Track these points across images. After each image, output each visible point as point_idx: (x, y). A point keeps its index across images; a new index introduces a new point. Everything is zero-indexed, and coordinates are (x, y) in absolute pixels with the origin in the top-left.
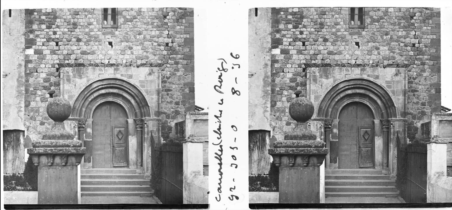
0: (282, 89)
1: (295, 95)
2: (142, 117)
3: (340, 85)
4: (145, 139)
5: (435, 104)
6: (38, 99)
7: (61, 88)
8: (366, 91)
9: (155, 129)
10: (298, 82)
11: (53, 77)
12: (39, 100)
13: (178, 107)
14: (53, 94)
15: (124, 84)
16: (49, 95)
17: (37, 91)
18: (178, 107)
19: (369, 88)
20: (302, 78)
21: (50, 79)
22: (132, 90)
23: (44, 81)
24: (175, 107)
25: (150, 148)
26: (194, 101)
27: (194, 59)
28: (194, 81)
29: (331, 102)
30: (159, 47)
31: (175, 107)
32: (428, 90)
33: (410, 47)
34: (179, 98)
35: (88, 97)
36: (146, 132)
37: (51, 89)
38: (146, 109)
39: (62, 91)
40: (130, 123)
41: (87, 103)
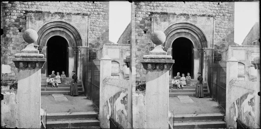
0: (9, 26)
1: (18, 30)
2: (202, 48)
3: (47, 25)
4: (78, 60)
5: (106, 38)
6: (11, 32)
7: (152, 28)
8: (64, 29)
9: (210, 55)
10: (146, 24)
11: (22, 19)
12: (12, 33)
13: (224, 42)
14: (146, 31)
15: (192, 27)
16: (144, 32)
17: (11, 27)
18: (99, 41)
19: (191, 29)
20: (148, 21)
21: (145, 21)
22: (72, 29)
23: (16, 21)
24: (222, 42)
25: (207, 67)
26: (109, 37)
27: (234, 14)
28: (234, 27)
29: (42, 35)
30: (214, 5)
31: (222, 42)
32: (226, 32)
33: (216, 4)
34: (225, 36)
35: (44, 33)
36: (80, 56)
37: (145, 28)
38: (80, 41)
39: (152, 29)
40: (70, 50)
41: (43, 36)
